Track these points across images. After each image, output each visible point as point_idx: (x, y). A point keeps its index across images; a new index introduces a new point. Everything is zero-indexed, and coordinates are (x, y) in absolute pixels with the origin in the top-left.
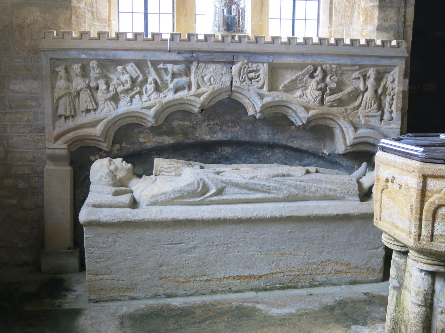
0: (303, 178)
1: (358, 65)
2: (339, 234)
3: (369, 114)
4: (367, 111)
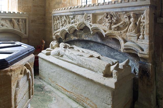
0: (87, 58)
1: (124, 11)
2: (92, 88)
3: (130, 35)
4: (130, 33)
